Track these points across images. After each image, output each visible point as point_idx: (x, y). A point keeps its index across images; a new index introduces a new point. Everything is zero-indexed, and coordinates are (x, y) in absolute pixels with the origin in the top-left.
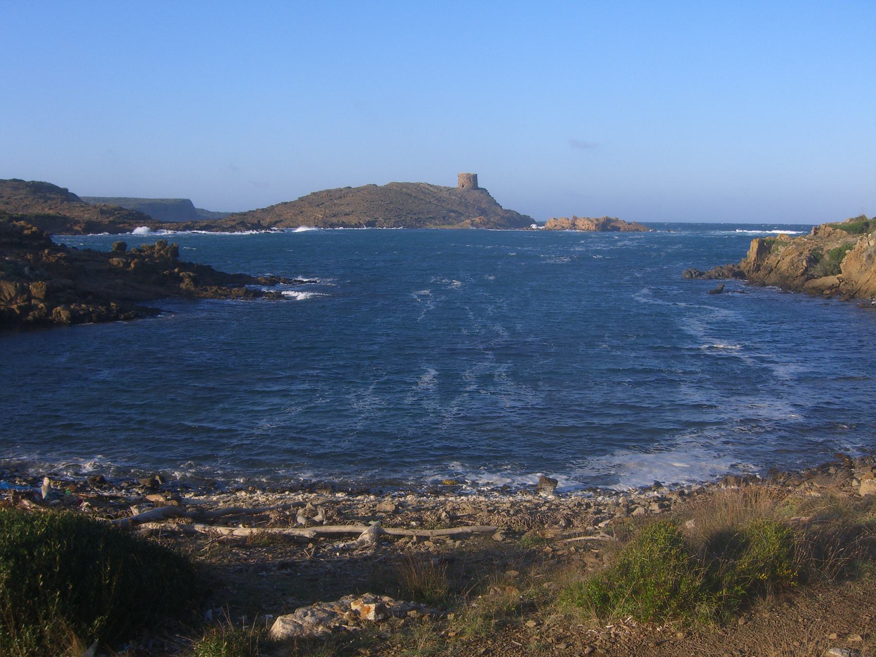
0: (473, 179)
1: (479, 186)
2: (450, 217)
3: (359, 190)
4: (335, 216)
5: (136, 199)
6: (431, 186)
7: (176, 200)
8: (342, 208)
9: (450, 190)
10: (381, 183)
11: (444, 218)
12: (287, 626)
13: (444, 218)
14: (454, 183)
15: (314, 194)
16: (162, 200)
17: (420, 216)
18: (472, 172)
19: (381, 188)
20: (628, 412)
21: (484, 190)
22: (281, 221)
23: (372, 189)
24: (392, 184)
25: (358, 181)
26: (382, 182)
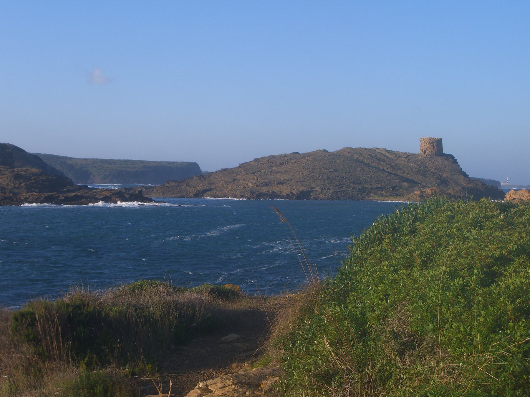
0: (438, 143)
1: (445, 151)
2: (401, 187)
3: (305, 156)
4: (266, 185)
5: (142, 162)
6: (388, 152)
7: (182, 163)
8: (278, 176)
9: (409, 157)
10: (332, 148)
11: (394, 188)
12: (46, 380)
13: (394, 188)
14: (414, 147)
15: (256, 160)
16: (169, 163)
17: (366, 186)
18: (437, 136)
19: (332, 154)
20: (202, 313)
21: (451, 158)
22: (211, 190)
23: (322, 156)
24: (344, 150)
25: (307, 145)
26: (333, 146)
